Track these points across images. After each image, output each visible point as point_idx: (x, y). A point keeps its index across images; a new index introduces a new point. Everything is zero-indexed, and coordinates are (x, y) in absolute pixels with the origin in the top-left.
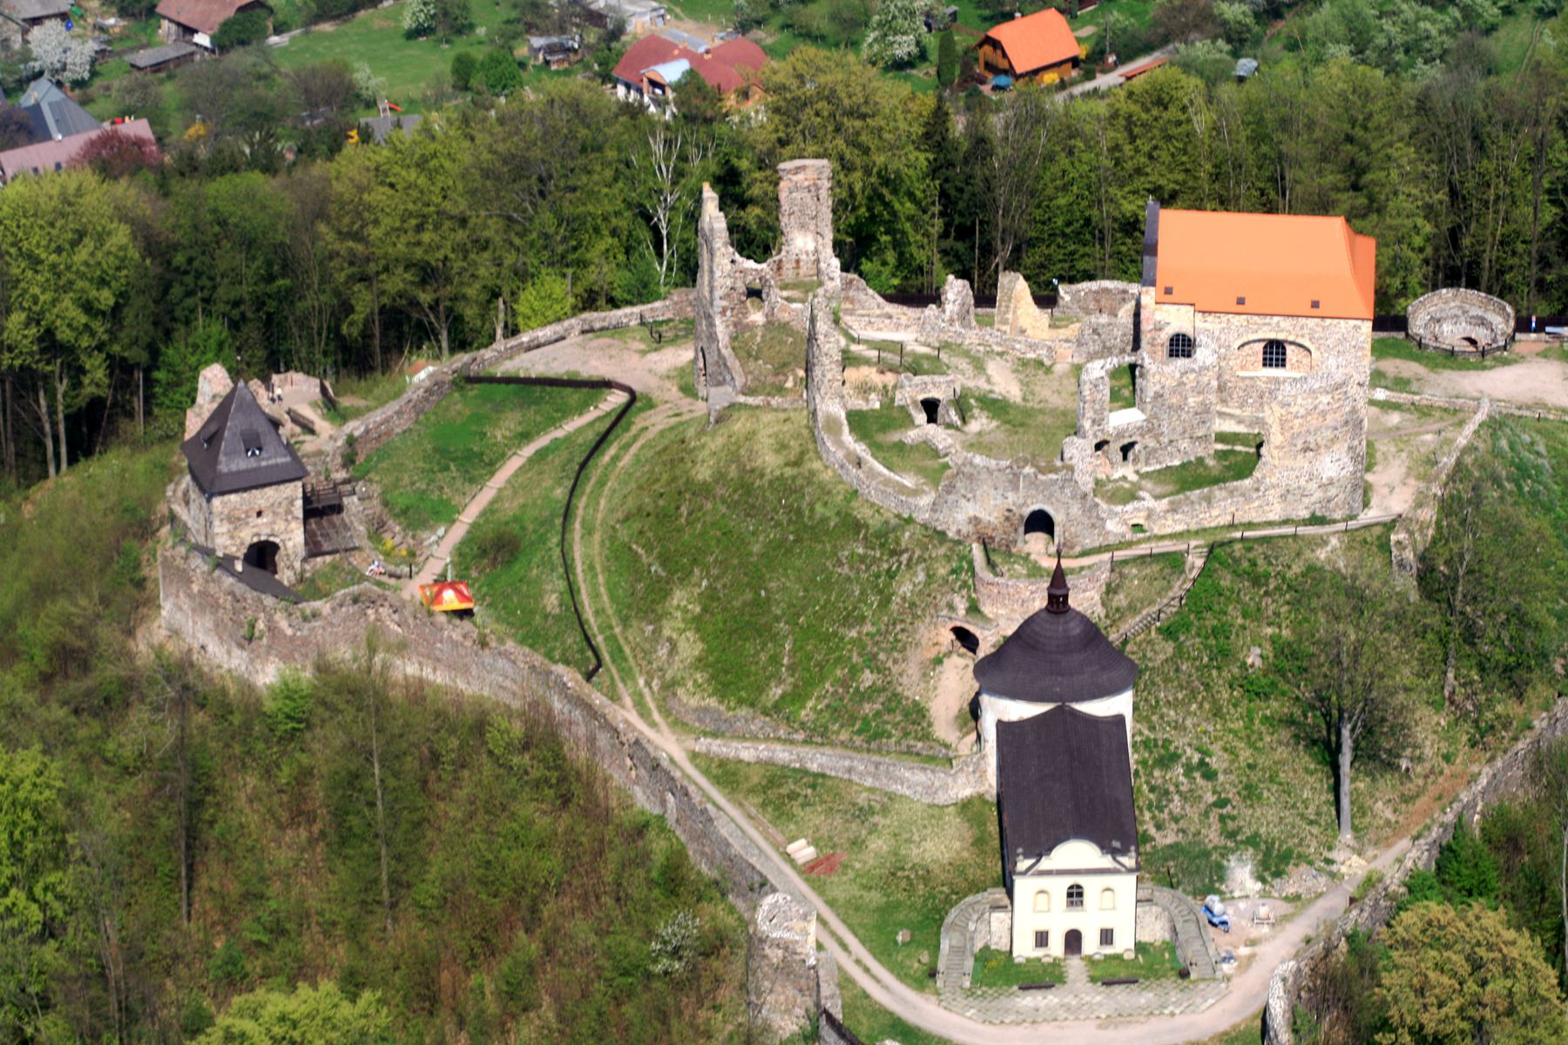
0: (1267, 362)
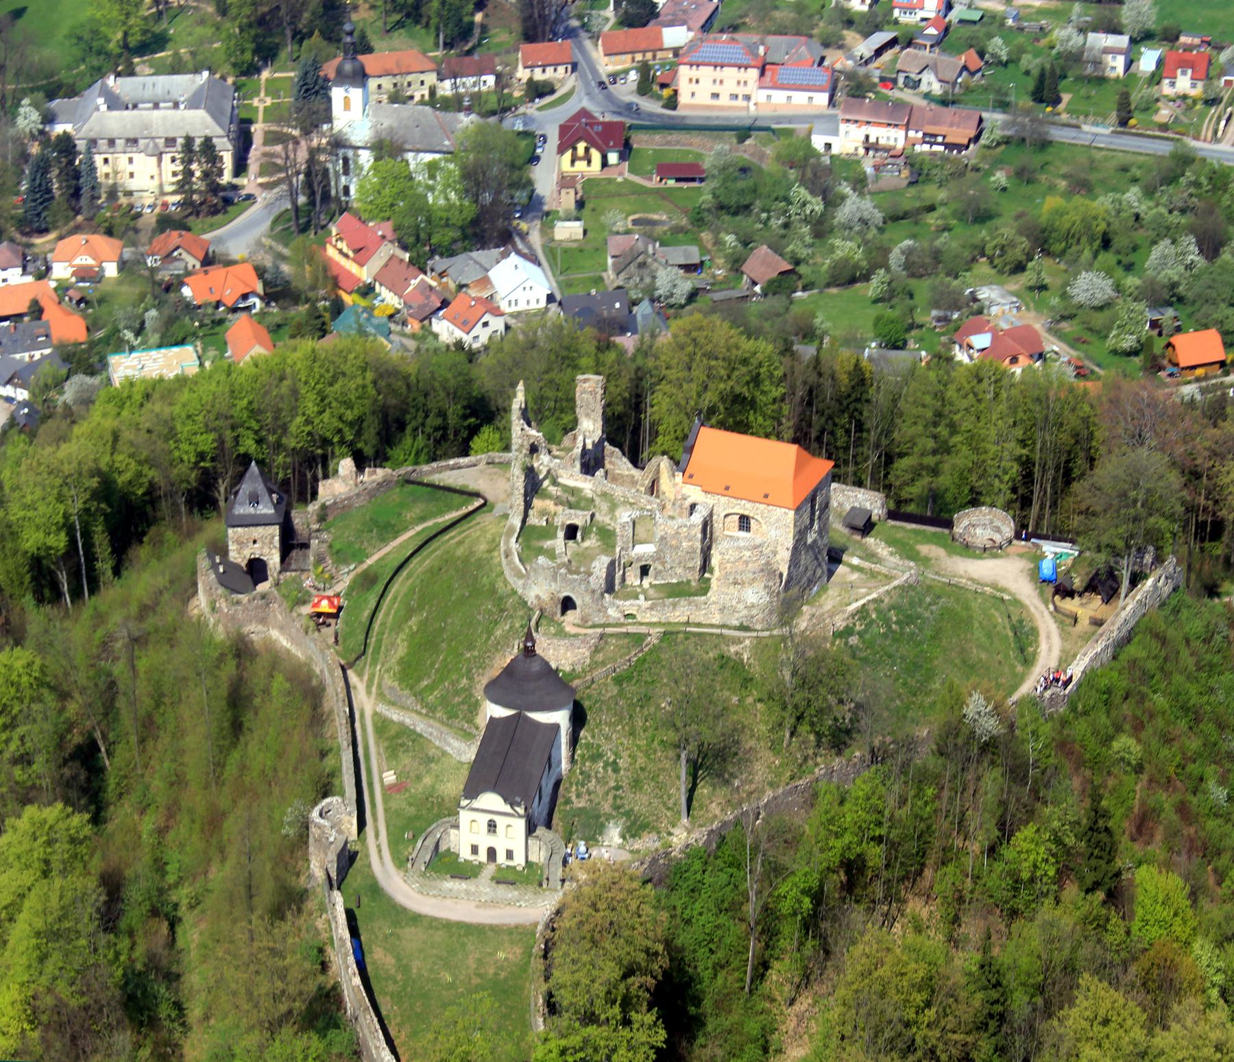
0: (741, 528)
